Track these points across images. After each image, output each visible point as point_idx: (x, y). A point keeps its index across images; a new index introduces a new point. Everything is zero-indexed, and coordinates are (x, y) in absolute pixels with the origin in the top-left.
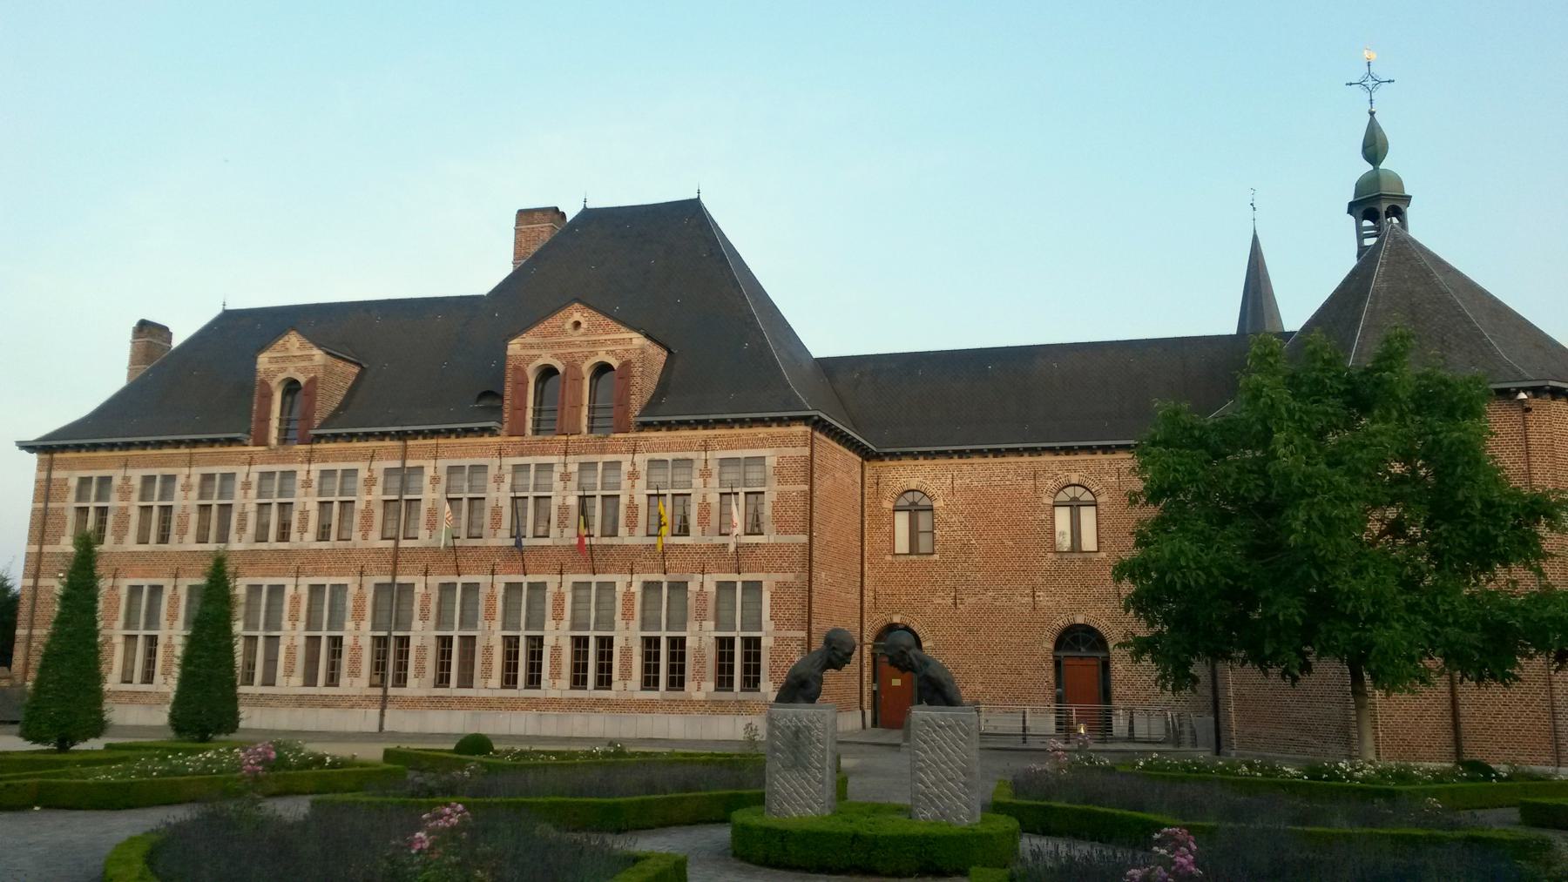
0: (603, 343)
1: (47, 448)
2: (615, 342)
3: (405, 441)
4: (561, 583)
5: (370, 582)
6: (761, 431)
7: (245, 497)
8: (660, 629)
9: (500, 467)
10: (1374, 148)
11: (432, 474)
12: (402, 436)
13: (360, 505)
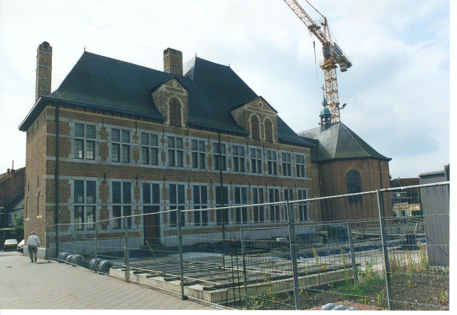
1: (24, 128)
4: (267, 189)
6: (303, 148)
7: (163, 146)
8: (199, 203)
9: (247, 148)
11: (228, 147)
13: (207, 156)
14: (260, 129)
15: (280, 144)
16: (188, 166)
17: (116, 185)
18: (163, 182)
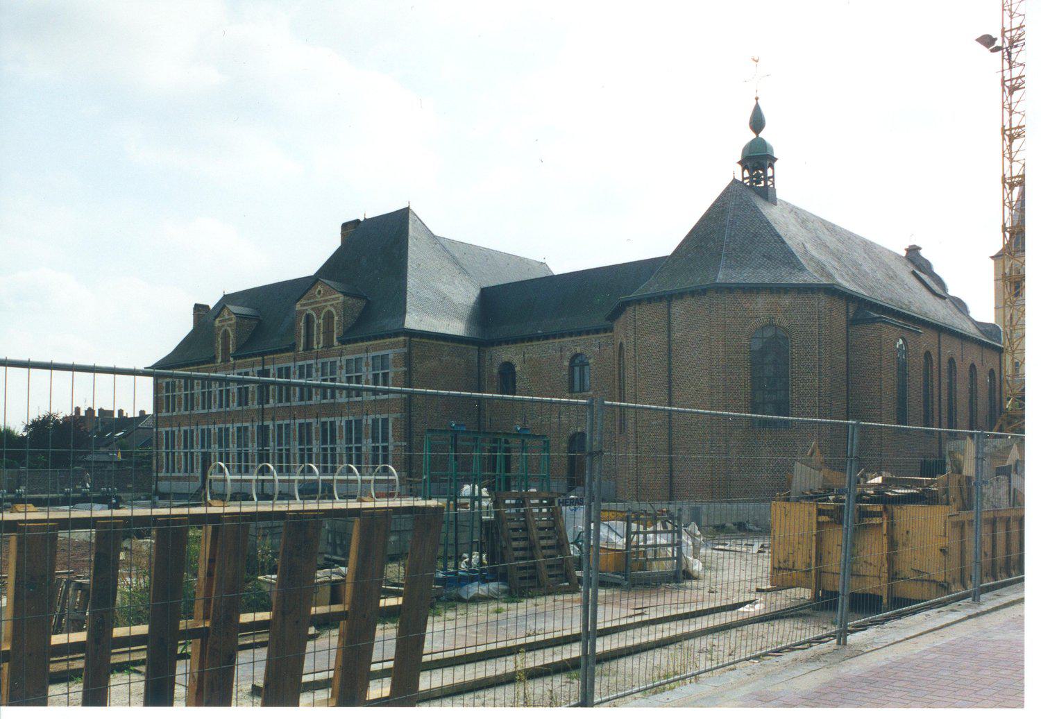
0: (328, 300)
1: (913, 252)
2: (334, 299)
3: (411, 338)
5: (256, 424)
6: (388, 341)
10: (757, 122)
12: (262, 354)
14: (315, 333)
15: (344, 346)
16: (234, 406)
17: (186, 432)
18: (213, 426)
